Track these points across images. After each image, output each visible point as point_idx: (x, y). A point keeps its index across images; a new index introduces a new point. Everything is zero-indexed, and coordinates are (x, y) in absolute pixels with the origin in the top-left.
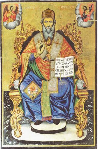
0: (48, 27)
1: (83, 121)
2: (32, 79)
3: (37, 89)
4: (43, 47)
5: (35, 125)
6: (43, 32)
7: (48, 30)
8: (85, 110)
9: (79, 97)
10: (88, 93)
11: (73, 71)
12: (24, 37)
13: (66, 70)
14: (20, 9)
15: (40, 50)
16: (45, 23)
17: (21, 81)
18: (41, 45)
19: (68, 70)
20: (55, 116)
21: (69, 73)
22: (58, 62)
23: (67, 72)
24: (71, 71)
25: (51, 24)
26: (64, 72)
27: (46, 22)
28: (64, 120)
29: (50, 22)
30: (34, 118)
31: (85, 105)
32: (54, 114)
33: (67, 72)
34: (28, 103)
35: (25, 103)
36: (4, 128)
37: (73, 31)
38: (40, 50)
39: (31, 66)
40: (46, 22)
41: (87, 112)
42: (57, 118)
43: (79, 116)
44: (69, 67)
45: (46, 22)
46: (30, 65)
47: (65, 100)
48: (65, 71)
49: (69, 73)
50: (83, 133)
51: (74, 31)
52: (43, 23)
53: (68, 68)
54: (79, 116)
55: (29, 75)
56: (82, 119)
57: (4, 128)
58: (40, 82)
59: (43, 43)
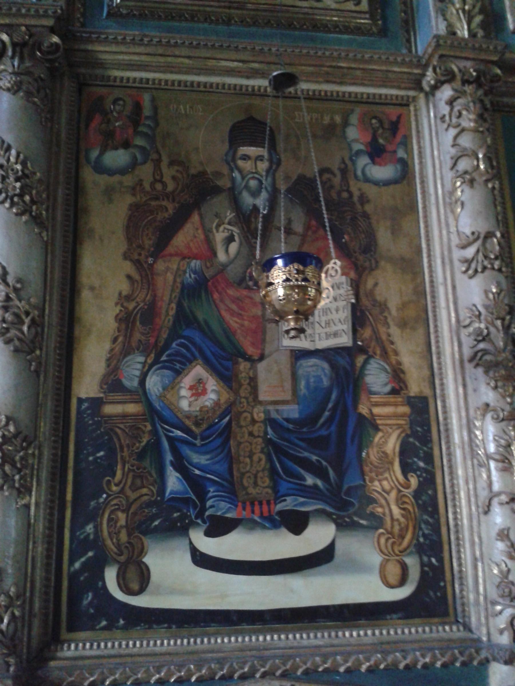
0: (251, 176)
1: (402, 520)
2: (197, 353)
3: (213, 391)
4: (234, 241)
5: (211, 539)
6: (232, 189)
7: (253, 183)
8: (405, 473)
9: (379, 422)
10: (405, 409)
11: (347, 327)
12: (477, 325)
13: (323, 325)
14: (147, 111)
15: (227, 251)
16: (240, 163)
17: (149, 361)
18: (226, 234)
19: (328, 323)
20: (289, 499)
21: (336, 335)
22: (324, 319)
23: (328, 330)
24: (340, 327)
25: (262, 166)
26: (317, 331)
27: (244, 159)
28: (328, 516)
29: (260, 158)
30: (203, 509)
31: (402, 453)
32: (284, 487)
33: (328, 330)
34: (178, 444)
35: (166, 444)
36: (71, 562)
37: (152, 185)
38: (227, 251)
39: (191, 312)
40: (246, 157)
41: (414, 481)
42: (295, 508)
43: (386, 499)
44: (334, 312)
45: (246, 157)
46: (185, 304)
47: (324, 432)
48: (317, 325)
49: (336, 335)
50: (404, 568)
51: (345, 195)
52: (234, 160)
53: (330, 317)
54: (386, 499)
55: (184, 337)
56: (396, 511)
57: (71, 562)
58: (229, 364)
59: (236, 230)
